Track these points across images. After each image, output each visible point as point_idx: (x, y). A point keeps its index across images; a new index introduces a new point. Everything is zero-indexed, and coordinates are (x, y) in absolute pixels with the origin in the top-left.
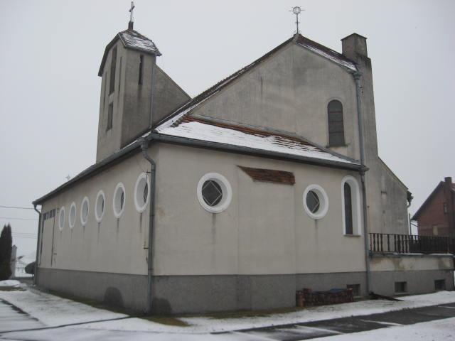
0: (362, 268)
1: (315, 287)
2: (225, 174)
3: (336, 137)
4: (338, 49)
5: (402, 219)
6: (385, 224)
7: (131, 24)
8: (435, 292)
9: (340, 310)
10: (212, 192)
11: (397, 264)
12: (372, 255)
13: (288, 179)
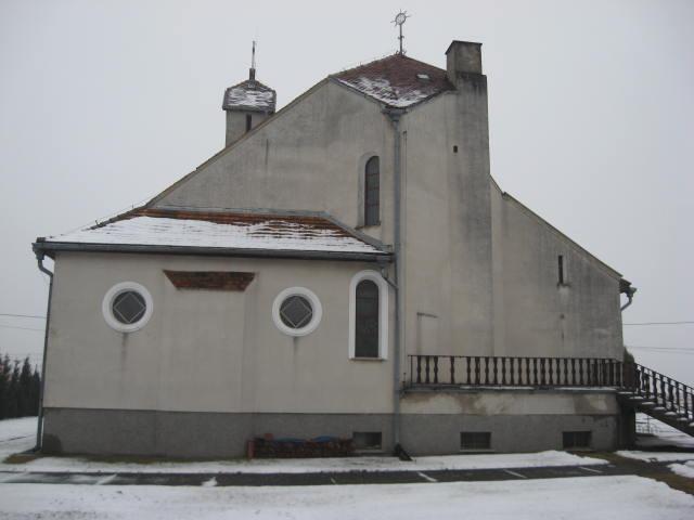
2: (147, 283)
3: (371, 217)
4: (441, 62)
6: (563, 337)
7: (252, 73)
9: (390, 463)
10: (129, 306)
12: (406, 390)
13: (239, 282)
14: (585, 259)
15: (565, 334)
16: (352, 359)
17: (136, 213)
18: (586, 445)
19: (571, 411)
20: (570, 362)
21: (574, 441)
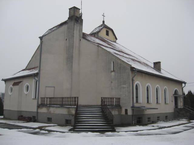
0: (34, 109)
1: (25, 115)
5: (125, 84)
6: (112, 89)
7: (104, 22)
8: (102, 132)
11: (48, 110)
12: (39, 106)
14: (119, 61)
15: (113, 88)
16: (33, 99)
17: (23, 70)
18: (51, 121)
19: (67, 113)
20: (109, 98)
21: (67, 123)
